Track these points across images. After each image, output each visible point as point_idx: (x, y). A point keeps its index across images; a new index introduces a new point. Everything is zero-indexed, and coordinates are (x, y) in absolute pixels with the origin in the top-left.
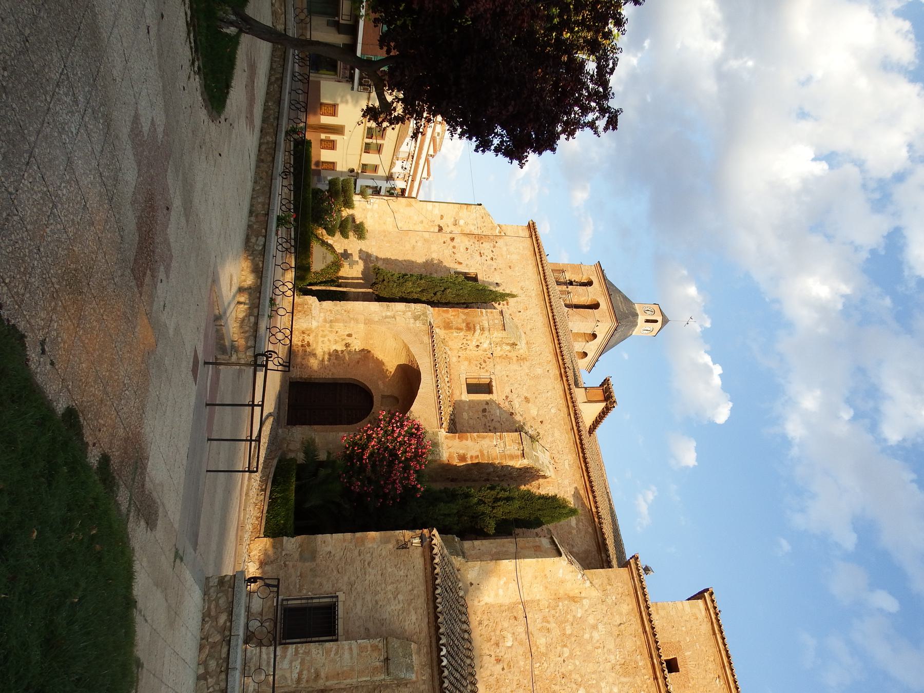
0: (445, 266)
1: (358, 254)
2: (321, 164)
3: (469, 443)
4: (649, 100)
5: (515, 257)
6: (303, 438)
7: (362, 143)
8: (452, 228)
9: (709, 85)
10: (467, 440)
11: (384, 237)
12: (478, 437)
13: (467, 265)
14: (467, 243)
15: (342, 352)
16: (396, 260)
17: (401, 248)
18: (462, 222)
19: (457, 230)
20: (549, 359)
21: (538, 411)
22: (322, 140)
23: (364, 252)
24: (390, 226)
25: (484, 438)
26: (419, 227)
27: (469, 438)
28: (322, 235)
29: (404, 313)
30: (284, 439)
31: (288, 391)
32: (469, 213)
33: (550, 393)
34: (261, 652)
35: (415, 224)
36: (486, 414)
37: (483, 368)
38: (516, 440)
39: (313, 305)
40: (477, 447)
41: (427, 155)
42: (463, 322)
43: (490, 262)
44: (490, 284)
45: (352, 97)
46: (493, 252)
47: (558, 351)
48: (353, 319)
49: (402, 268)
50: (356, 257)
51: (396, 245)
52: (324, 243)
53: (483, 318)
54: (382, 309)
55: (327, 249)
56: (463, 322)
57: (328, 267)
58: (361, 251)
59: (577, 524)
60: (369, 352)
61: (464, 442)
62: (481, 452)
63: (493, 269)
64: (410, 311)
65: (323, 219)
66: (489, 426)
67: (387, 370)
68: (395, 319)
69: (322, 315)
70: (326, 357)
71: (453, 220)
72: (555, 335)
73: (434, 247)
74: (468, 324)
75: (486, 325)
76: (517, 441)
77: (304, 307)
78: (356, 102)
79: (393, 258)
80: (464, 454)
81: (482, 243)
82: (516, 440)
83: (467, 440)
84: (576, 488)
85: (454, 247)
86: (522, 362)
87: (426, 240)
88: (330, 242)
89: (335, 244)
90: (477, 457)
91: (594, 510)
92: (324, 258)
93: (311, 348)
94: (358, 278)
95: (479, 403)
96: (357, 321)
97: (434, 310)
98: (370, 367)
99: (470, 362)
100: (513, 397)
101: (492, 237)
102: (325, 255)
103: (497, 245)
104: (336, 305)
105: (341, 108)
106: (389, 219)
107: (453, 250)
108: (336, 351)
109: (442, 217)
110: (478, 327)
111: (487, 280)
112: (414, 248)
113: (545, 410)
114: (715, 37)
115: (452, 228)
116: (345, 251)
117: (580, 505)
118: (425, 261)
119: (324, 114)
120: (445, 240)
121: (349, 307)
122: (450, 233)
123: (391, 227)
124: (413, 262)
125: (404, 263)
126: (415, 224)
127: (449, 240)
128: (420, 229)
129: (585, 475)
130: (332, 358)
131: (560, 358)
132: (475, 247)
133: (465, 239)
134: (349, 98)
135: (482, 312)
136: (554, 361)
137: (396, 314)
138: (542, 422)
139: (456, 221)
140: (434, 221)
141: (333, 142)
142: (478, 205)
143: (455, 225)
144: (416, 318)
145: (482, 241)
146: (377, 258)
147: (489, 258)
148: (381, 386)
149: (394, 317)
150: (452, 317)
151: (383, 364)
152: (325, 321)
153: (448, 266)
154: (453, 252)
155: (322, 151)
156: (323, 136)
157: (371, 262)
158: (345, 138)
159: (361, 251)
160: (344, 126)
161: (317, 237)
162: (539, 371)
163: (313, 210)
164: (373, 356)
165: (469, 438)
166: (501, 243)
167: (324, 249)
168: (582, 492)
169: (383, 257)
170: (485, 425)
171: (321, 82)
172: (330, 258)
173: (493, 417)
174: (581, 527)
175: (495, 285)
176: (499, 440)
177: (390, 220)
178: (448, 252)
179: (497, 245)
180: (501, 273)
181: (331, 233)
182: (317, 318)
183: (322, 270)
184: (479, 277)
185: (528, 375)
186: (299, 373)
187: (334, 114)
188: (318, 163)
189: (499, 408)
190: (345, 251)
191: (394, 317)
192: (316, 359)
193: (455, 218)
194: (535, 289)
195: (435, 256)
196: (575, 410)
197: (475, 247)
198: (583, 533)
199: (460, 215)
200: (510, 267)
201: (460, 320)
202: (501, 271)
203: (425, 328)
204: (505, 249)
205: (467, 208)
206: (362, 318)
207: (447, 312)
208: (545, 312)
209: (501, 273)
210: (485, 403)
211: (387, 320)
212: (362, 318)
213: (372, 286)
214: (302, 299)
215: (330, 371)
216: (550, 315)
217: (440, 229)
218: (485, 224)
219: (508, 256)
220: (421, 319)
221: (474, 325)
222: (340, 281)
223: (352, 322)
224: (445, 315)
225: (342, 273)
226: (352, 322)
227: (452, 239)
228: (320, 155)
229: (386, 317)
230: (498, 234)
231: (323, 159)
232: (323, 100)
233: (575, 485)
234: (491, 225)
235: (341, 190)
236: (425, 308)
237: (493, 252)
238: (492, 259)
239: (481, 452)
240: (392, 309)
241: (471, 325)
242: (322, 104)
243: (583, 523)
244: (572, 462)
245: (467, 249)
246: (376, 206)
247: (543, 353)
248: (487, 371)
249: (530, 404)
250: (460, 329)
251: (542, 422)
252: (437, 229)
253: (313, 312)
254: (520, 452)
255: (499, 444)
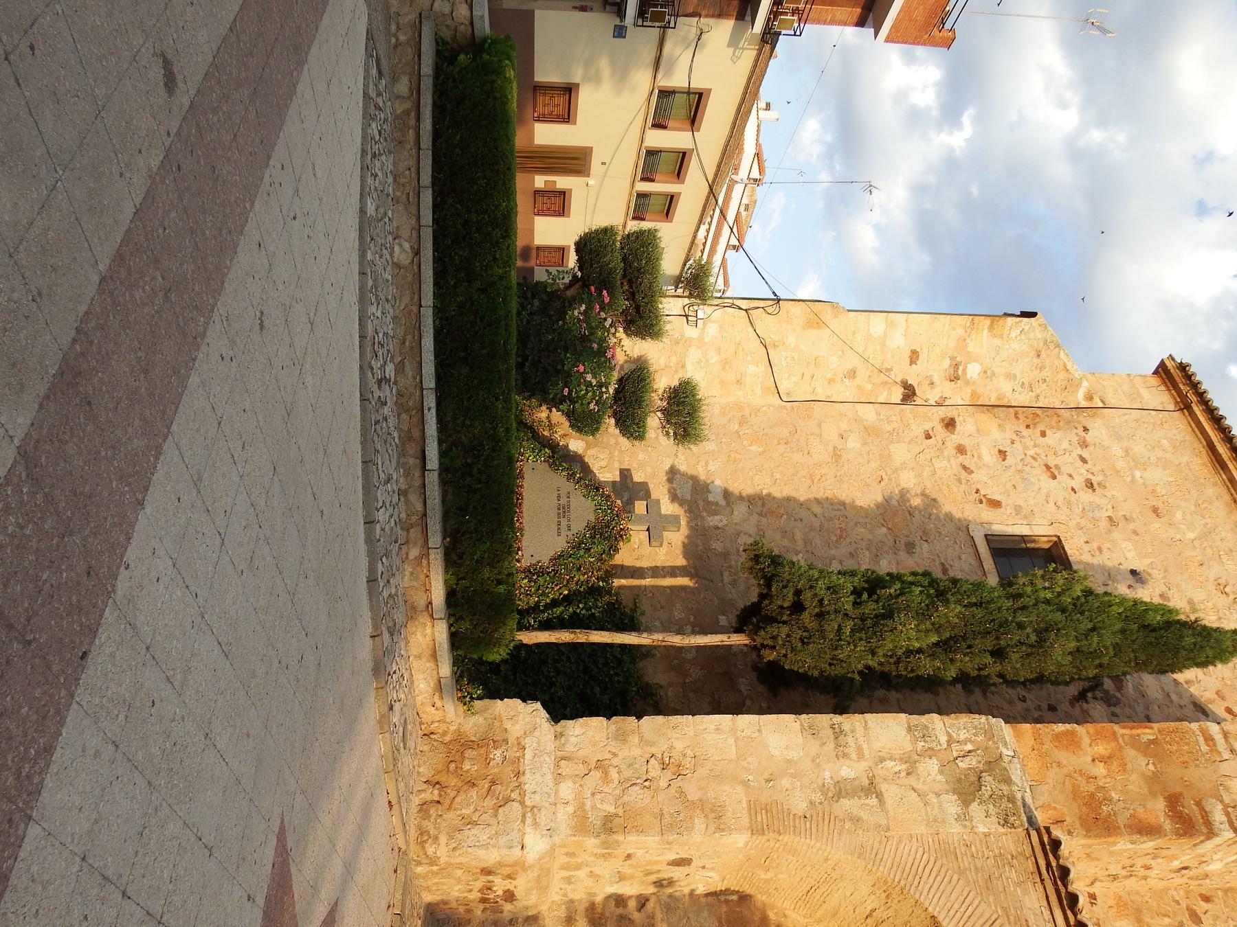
0: (949, 517)
1: (667, 486)
2: (534, 253)
4: (975, 191)
5: (1157, 476)
7: (631, 194)
8: (944, 389)
9: (1062, 172)
11: (740, 424)
13: (1018, 509)
14: (997, 434)
15: (643, 902)
16: (789, 499)
17: (797, 457)
18: (973, 371)
19: (958, 395)
22: (537, 192)
23: (684, 475)
24: (755, 393)
26: (846, 391)
28: (551, 426)
29: (911, 764)
32: (997, 341)
34: (518, 157)
35: (831, 381)
39: (529, 742)
41: (728, 246)
43: (1085, 496)
44: (1110, 574)
45: (613, 63)
46: (1084, 461)
48: (702, 804)
49: (812, 528)
50: (660, 492)
51: (782, 448)
52: (561, 458)
54: (814, 746)
55: (571, 477)
56: (1153, 794)
57: (577, 547)
58: (673, 473)
63: (1104, 524)
65: (568, 378)
68: (879, 796)
69: (567, 790)
71: (947, 363)
73: (901, 453)
77: (488, 761)
78: (622, 74)
79: (778, 495)
81: (1043, 434)
85: (961, 450)
87: (870, 432)
88: (576, 444)
89: (591, 452)
92: (563, 511)
93: (519, 904)
94: (673, 572)
96: (716, 817)
97: (1018, 736)
101: (1066, 414)
102: (563, 501)
103: (1089, 437)
104: (622, 737)
105: (586, 99)
106: (752, 369)
107: (961, 458)
109: (914, 356)
111: (1096, 561)
112: (836, 456)
114: (1063, 105)
115: (944, 389)
116: (625, 474)
118: (880, 499)
119: (542, 119)
120: (928, 426)
121: (679, 746)
122: (939, 405)
123: (759, 392)
124: (843, 504)
125: (817, 509)
126: (831, 381)
127: (939, 428)
128: (848, 396)
132: (1026, 448)
133: (989, 422)
134: (604, 63)
137: (879, 771)
139: (957, 366)
140: (889, 370)
141: (563, 194)
142: (1025, 315)
143: (954, 378)
145: (1041, 427)
146: (727, 494)
147: (1078, 483)
152: (581, 825)
153: (957, 514)
154: (965, 468)
155: (537, 218)
156: (540, 181)
157: (712, 509)
158: (591, 182)
159: (673, 473)
160: (591, 149)
161: (536, 437)
163: (523, 340)
166: (1098, 430)
167: (559, 480)
169: (748, 490)
171: (538, 13)
172: (584, 511)
175: (1131, 580)
177: (755, 370)
178: (947, 465)
179: (1089, 437)
180: (1135, 532)
181: (585, 423)
183: (556, 559)
184: (1075, 550)
187: (566, 117)
188: (526, 252)
190: (625, 474)
191: (871, 788)
193: (953, 358)
195: (908, 480)
197: (1026, 448)
199: (971, 348)
200: (1155, 510)
201: (1136, 785)
202: (1132, 526)
204: (1117, 450)
205: (991, 328)
206: (734, 798)
207: (1071, 743)
209: (1135, 532)
211: (846, 804)
212: (734, 798)
213: (749, 619)
214: (479, 719)
217: (909, 394)
218: (1045, 374)
219: (1138, 474)
220: (986, 791)
222: (617, 582)
225: (625, 556)
227: (950, 424)
228: (532, 231)
229: (841, 790)
230: (1084, 404)
231: (540, 240)
232: (541, 77)
234: (1062, 375)
235: (620, 272)
236: (989, 734)
237: (1084, 461)
238: (1090, 485)
240: (859, 749)
241: (1190, 808)
242: (539, 88)
245: (1003, 454)
246: (712, 330)
250: (1145, 829)
252: (897, 394)
253: (531, 781)
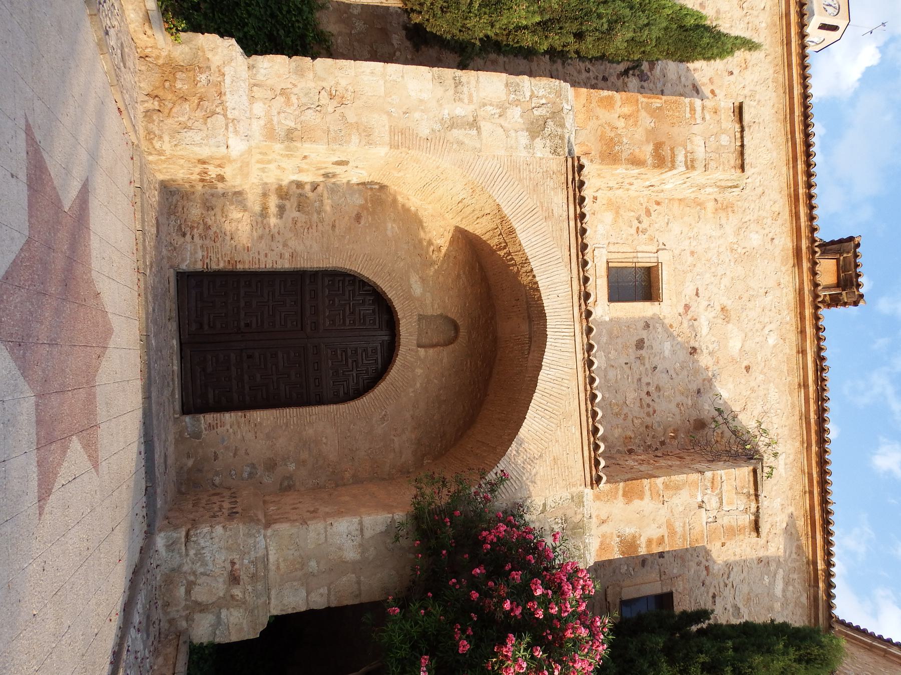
3: (646, 504)
6: (233, 563)
10: (642, 499)
12: (666, 486)
15: (315, 187)
20: (776, 208)
21: (744, 341)
25: (678, 488)
27: (647, 493)
30: (177, 570)
31: (174, 314)
33: (770, 297)
36: (643, 352)
37: (644, 231)
38: (743, 487)
40: (663, 513)
42: (648, 141)
47: (802, 191)
53: (695, 129)
54: (440, 91)
59: (784, 591)
60: (383, 187)
61: (637, 503)
62: (670, 526)
64: (517, 103)
66: (648, 384)
67: (430, 243)
68: (479, 129)
69: (259, 108)
70: (273, 202)
72: (800, 148)
74: (658, 146)
75: (700, 153)
76: (745, 491)
80: (634, 537)
82: (743, 487)
83: (642, 499)
84: (791, 516)
86: (723, 214)
90: (661, 541)
91: (821, 565)
95: (629, 325)
96: (367, 135)
97: (577, 96)
98: (389, 233)
99: (617, 213)
100: (699, 308)
108: (299, 185)
110: (680, 158)
113: (757, 340)
117: (794, 550)
121: (343, 83)
129: (816, 491)
130: (288, 204)
131: (803, 211)
135: (693, 110)
136: (786, 215)
137: (481, 113)
138: (748, 368)
144: (536, 129)
148: (417, 289)
149: (474, 124)
150: (621, 123)
151: (420, 223)
162: (755, 239)
164: (395, 201)
165: (647, 493)
168: (801, 523)
170: (640, 380)
173: (656, 361)
174: (789, 594)
176: (709, 491)
182: (241, 128)
185: (732, 250)
186: (200, 255)
189: (670, 335)
192: (245, 209)
194: (767, 8)
196: (820, 349)
198: (790, 607)
201: (640, 134)
203: (557, 164)
206: (380, 124)
208: (781, 78)
210: (642, 324)
211: (455, 132)
212: (380, 124)
214: (185, 48)
215: (285, 245)
216: (797, 90)
220: (547, 131)
221: (672, 149)
223: (355, 139)
224: (605, 115)
226: (355, 139)
229: (453, 123)
233: (791, 509)
236: (559, 94)
239: (670, 526)
241: (666, 152)
243: (794, 587)
244: (792, 457)
247: (766, 191)
248: (651, 239)
249: (730, 326)
250: (636, 162)
251: (748, 368)
253: (231, 100)
254: (748, 519)
255: (709, 499)
